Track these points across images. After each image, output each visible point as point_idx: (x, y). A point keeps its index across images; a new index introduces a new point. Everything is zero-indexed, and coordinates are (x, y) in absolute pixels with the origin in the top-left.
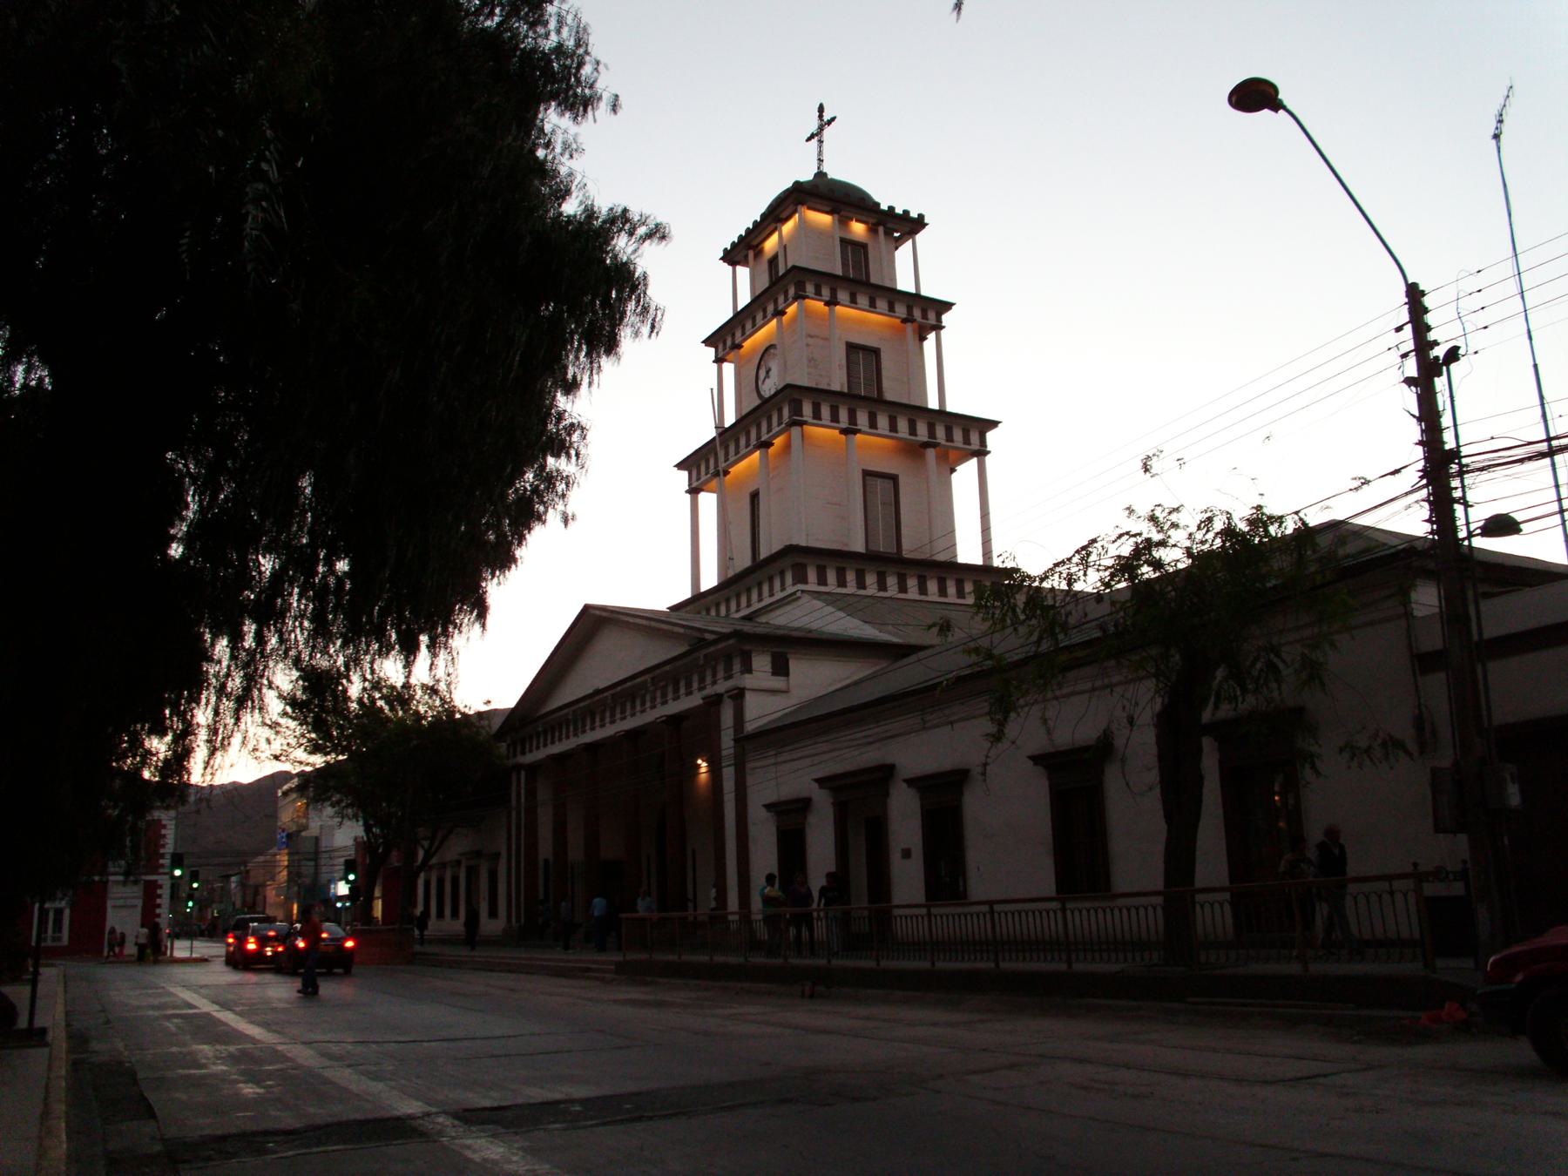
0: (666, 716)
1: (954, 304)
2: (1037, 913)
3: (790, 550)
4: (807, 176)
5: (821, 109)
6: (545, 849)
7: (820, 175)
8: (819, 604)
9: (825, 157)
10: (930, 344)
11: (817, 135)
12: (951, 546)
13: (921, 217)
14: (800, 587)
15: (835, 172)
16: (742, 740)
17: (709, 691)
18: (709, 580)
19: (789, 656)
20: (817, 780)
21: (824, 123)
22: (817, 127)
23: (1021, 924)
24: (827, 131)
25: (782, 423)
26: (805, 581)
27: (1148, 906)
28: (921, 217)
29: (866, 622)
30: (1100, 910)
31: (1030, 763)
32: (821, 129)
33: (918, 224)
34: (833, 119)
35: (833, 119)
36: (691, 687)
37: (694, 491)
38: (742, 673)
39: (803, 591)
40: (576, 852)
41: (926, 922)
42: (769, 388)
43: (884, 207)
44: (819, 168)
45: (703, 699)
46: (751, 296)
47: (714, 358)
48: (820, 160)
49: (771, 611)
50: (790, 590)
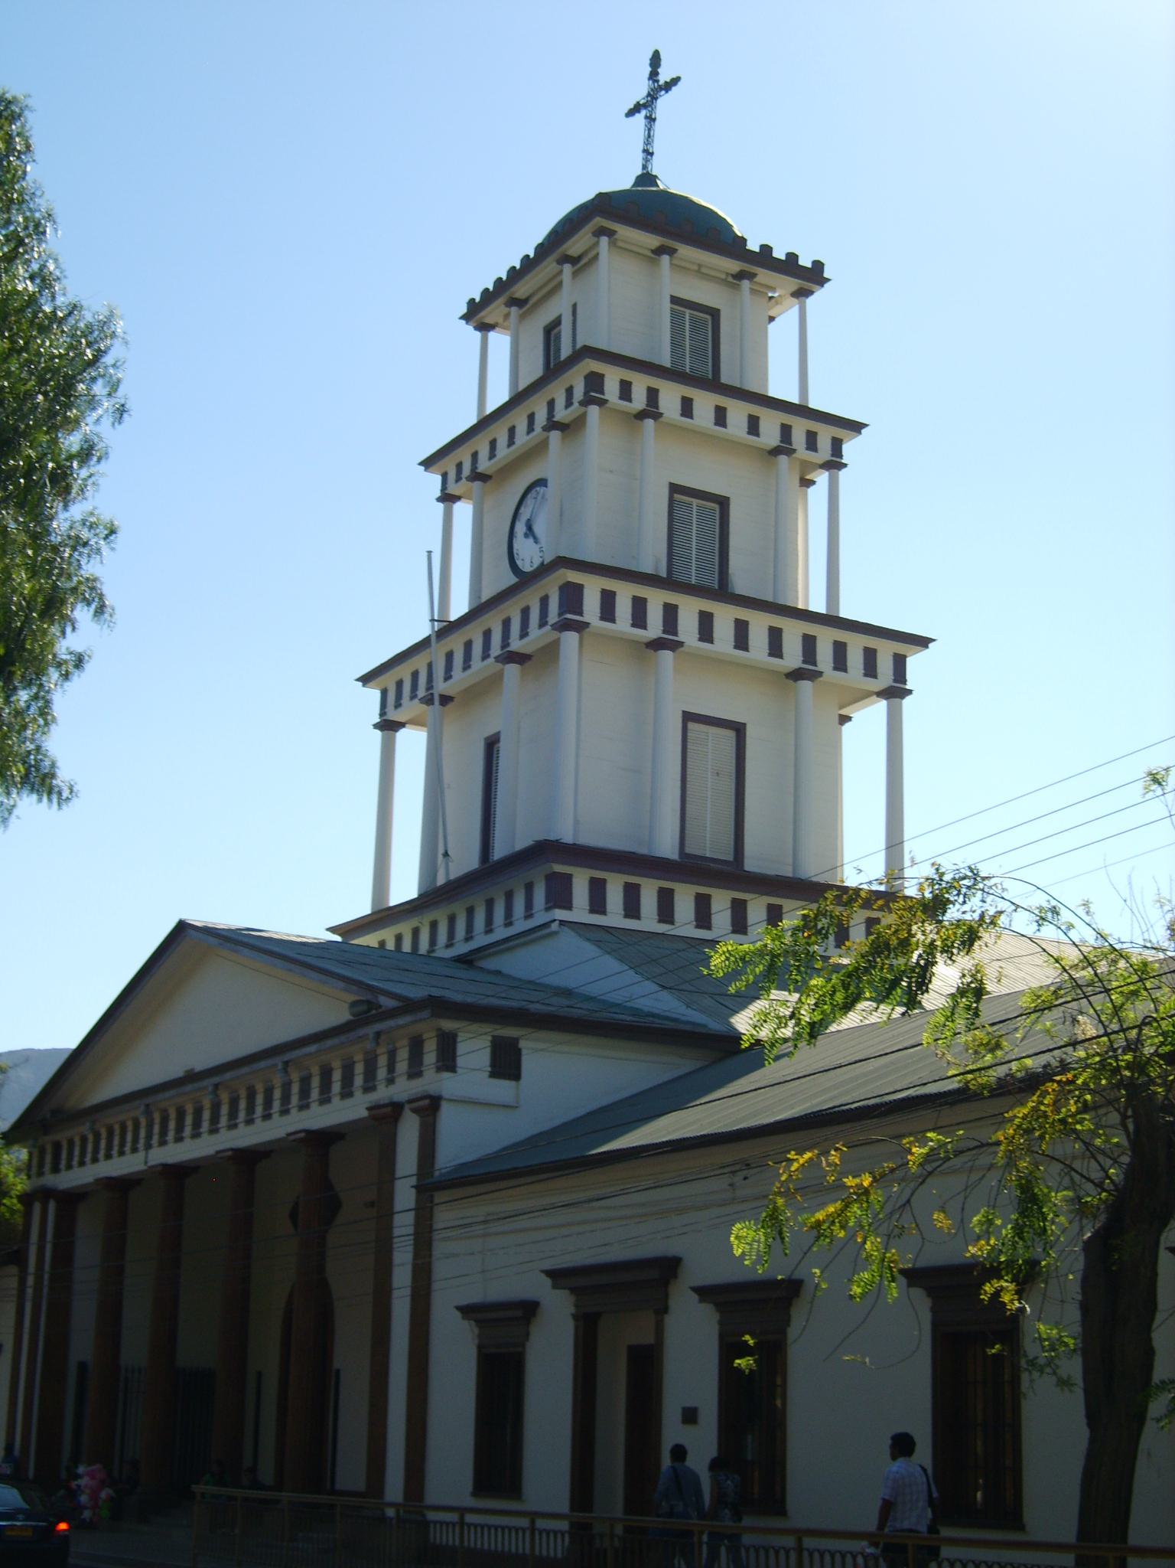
0: (232, 1149)
1: (866, 425)
2: (838, 1557)
3: (545, 850)
4: (621, 179)
5: (656, 60)
6: (82, 1346)
7: (646, 178)
8: (590, 949)
9: (657, 147)
10: (818, 494)
11: (645, 107)
12: (889, 847)
13: (818, 266)
14: (560, 914)
15: (672, 180)
16: (429, 1186)
17: (383, 1093)
18: (404, 888)
19: (522, 1044)
20: (550, 1273)
21: (659, 88)
22: (645, 93)
23: (548, 1544)
24: (664, 102)
25: (488, 656)
26: (568, 905)
27: (980, 1563)
28: (818, 266)
29: (664, 987)
30: (849, 1555)
31: (458, 1314)
32: (653, 96)
33: (813, 276)
34: (675, 81)
35: (675, 81)
36: (254, 1113)
37: (388, 726)
38: (439, 1069)
39: (562, 923)
40: (135, 1349)
41: (528, 1539)
42: (529, 556)
43: (753, 246)
44: (644, 167)
45: (368, 1109)
46: (478, 416)
47: (438, 494)
48: (648, 153)
49: (508, 949)
50: (540, 918)
